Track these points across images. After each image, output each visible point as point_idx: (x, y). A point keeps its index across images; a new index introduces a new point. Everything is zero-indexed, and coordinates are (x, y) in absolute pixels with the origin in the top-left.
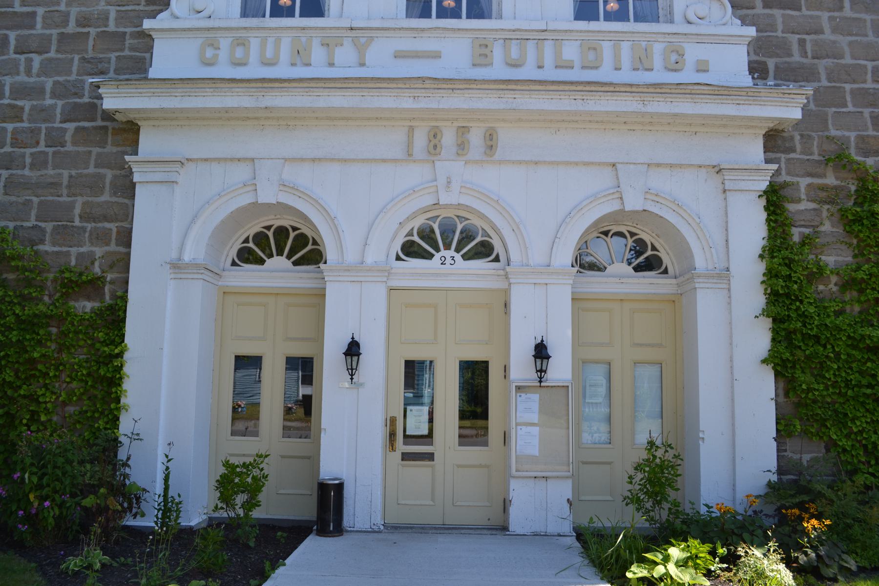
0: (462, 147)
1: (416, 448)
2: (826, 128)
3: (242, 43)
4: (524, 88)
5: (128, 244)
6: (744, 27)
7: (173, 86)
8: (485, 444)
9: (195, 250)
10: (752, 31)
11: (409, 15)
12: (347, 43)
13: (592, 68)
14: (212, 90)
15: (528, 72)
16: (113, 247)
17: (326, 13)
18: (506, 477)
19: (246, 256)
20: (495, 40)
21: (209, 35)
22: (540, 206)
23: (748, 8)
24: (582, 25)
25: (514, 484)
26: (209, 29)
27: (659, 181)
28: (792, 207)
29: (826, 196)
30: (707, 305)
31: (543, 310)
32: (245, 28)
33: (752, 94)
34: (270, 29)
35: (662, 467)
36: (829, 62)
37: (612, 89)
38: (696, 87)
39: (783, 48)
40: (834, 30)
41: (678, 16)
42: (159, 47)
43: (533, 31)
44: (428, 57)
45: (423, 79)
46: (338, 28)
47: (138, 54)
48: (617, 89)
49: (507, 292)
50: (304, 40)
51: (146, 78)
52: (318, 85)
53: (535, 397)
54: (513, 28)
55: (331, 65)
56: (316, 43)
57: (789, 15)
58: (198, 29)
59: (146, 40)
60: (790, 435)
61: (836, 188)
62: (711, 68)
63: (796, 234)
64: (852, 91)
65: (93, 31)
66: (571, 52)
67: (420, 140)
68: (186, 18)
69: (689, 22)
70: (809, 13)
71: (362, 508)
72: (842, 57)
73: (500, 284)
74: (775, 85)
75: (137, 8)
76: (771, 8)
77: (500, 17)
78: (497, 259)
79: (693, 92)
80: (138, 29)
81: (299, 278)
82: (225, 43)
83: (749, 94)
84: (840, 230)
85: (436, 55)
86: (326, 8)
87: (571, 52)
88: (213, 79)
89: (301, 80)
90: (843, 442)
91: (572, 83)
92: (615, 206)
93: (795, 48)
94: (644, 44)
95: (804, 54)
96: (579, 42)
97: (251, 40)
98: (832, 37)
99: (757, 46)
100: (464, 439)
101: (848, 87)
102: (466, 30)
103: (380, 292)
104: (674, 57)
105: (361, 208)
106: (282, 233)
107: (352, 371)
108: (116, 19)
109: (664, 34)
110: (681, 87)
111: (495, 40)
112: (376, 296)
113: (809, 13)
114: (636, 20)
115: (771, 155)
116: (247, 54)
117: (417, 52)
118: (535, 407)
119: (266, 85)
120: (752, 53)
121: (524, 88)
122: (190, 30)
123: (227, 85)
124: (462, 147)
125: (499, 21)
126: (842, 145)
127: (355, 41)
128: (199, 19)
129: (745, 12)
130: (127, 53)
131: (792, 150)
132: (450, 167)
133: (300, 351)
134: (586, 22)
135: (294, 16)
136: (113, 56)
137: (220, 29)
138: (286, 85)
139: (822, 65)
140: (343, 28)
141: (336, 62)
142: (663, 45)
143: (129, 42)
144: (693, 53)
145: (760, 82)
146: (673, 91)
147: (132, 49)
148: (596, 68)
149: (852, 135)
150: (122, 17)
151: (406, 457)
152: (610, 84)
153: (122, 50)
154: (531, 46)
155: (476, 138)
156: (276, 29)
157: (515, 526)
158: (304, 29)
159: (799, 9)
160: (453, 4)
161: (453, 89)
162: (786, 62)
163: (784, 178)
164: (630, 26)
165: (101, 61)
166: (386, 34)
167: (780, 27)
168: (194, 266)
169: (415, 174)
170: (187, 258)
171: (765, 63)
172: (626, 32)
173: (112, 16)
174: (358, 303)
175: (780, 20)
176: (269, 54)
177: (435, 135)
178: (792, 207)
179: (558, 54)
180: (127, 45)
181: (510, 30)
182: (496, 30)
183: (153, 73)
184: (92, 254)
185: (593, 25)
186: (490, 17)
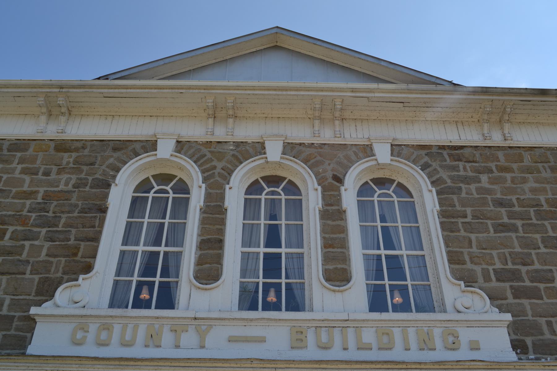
3: (107, 328)
4: (333, 367)
6: (502, 314)
7: (46, 362)
10: (508, 317)
11: (241, 308)
12: (191, 330)
13: (387, 349)
14: (77, 366)
15: (336, 353)
17: (176, 306)
20: (309, 327)
23: (502, 299)
24: (376, 316)
26: (82, 316)
32: (111, 316)
33: (518, 367)
34: (131, 317)
37: (404, 366)
38: (472, 363)
39: (535, 329)
41: (449, 307)
42: (40, 330)
43: (337, 320)
44: (256, 341)
45: (251, 360)
46: (185, 318)
47: (21, 333)
48: (409, 367)
50: (157, 326)
51: (24, 354)
52: (165, 364)
54: (322, 318)
55: (177, 347)
56: (166, 329)
57: (534, 303)
58: (73, 316)
59: (31, 323)
62: (481, 346)
66: (369, 336)
68: (65, 307)
69: (459, 312)
70: (549, 301)
74: (537, 359)
75: (27, 297)
76: (519, 298)
77: (312, 310)
79: (471, 367)
80: (26, 314)
82: (93, 328)
83: (517, 367)
85: (262, 340)
86: (176, 302)
87: (369, 336)
88: (80, 357)
89: (152, 360)
91: (372, 362)
93: (545, 328)
94: (426, 329)
96: (374, 329)
97: (115, 325)
99: (515, 328)
102: (286, 320)
104: (451, 339)
108: (9, 305)
109: (441, 321)
110: (460, 363)
111: (309, 327)
113: (549, 301)
114: (418, 311)
117: (247, 337)
119: (122, 363)
120: (512, 333)
121: (333, 367)
122: (66, 316)
123: (91, 362)
125: (311, 313)
128: (76, 308)
129: (499, 302)
130: (13, 332)
134: (378, 314)
135: (150, 308)
137: (91, 316)
138: (139, 363)
140: (188, 318)
141: (181, 345)
142: (442, 329)
143: (16, 323)
144: (466, 335)
145: (523, 357)
146: (454, 367)
147: (17, 329)
148: (390, 349)
150: (14, 305)
152: (403, 363)
153: (9, 330)
154: (337, 333)
156: (136, 317)
158: (158, 318)
159: (542, 299)
160: (275, 300)
161: (275, 368)
162: (540, 340)
164: (413, 316)
166: (223, 323)
167: (530, 313)
171: (523, 341)
172: (410, 321)
175: (528, 308)
179: (359, 338)
180: (14, 326)
181: (319, 320)
182: (309, 320)
183: (30, 350)
185: (384, 316)
186: (303, 310)
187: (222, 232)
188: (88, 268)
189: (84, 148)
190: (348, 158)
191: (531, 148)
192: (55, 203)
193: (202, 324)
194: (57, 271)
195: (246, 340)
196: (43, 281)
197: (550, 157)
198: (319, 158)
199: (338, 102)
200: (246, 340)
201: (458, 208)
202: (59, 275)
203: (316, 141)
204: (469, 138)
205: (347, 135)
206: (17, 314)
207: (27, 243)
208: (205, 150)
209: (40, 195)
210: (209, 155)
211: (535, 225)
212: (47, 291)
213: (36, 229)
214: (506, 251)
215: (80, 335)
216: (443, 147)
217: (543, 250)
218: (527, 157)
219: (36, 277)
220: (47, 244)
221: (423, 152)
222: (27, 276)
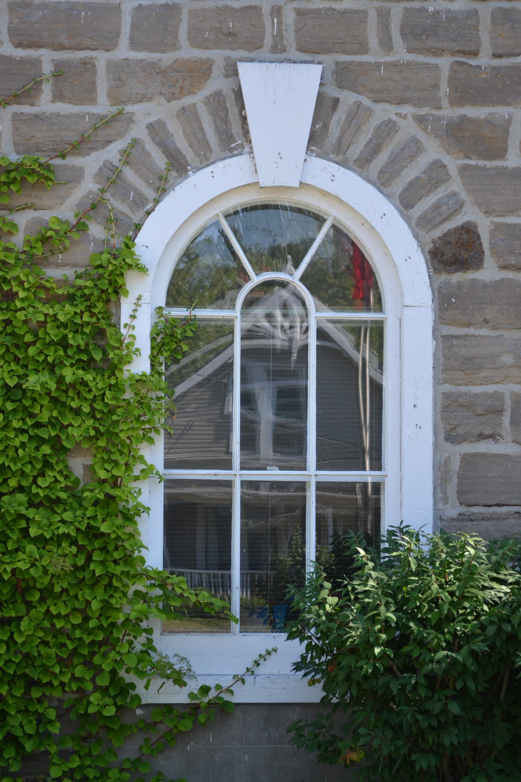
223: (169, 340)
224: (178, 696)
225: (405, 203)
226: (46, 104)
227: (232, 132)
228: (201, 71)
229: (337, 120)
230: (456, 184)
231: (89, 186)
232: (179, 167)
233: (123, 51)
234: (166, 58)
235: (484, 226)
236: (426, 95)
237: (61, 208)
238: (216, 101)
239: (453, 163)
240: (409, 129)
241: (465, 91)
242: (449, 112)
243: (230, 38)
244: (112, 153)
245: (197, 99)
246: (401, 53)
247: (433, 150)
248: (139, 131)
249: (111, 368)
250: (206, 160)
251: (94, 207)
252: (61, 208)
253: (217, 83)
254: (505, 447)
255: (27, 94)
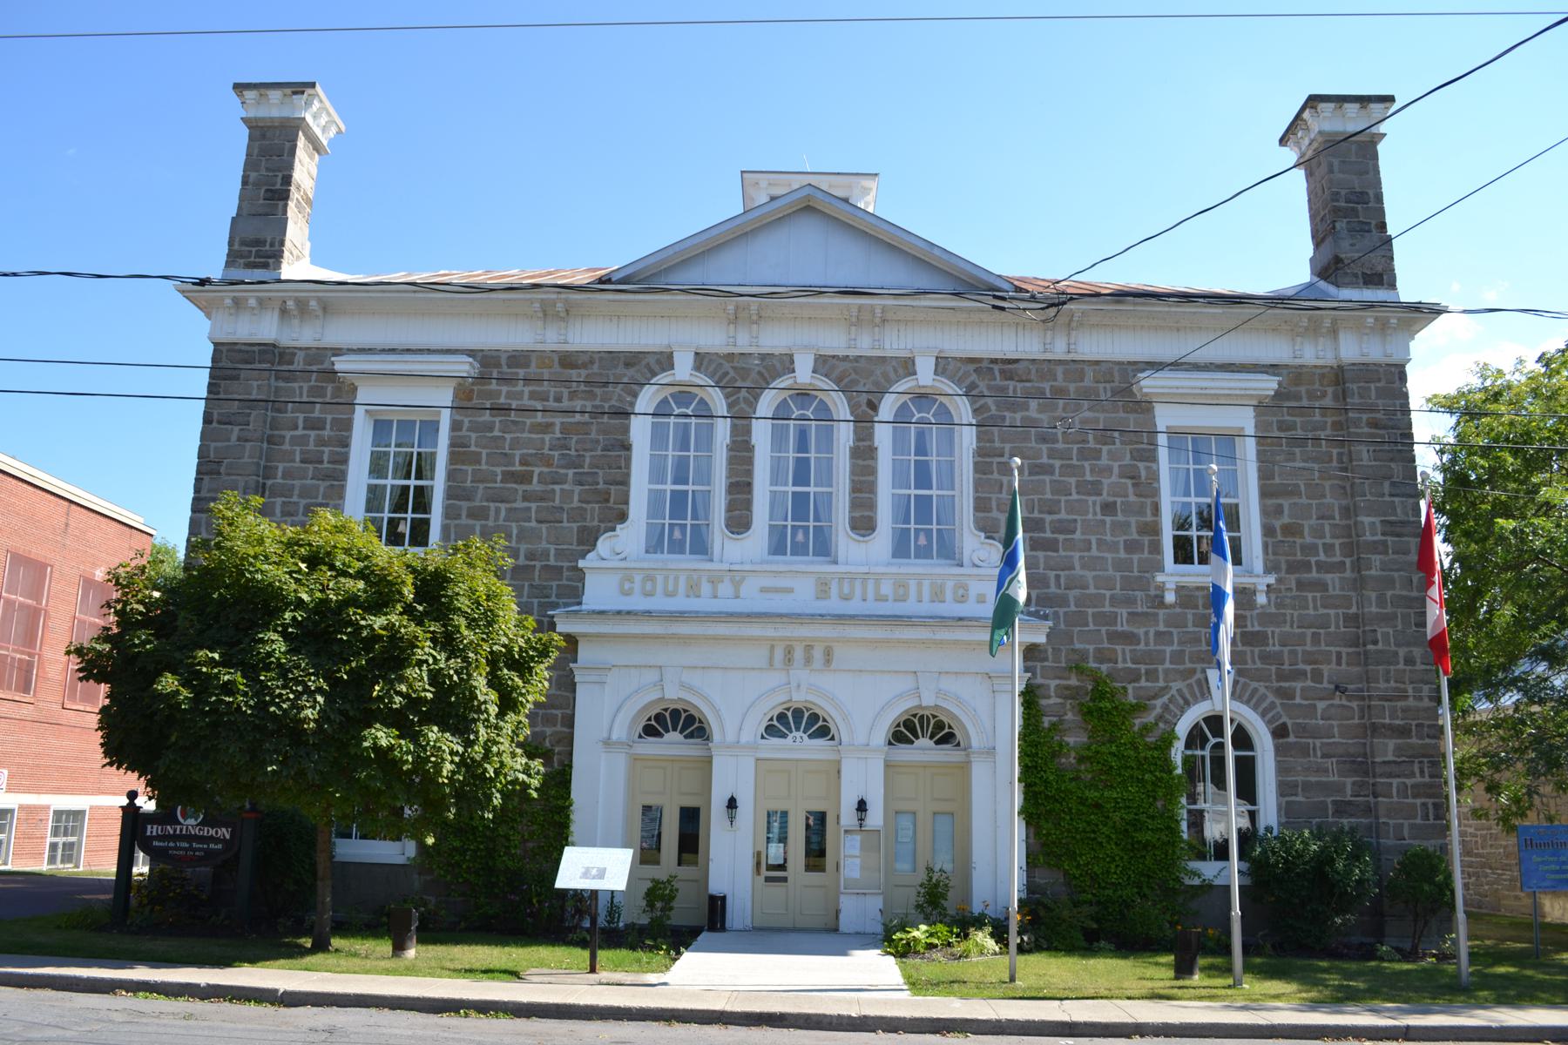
0: (808, 660)
1: (776, 872)
2: (1072, 642)
3: (652, 579)
5: (572, 726)
8: (823, 870)
9: (619, 733)
12: (727, 580)
16: (559, 728)
18: (838, 893)
19: (649, 731)
21: (627, 575)
22: (864, 702)
25: (843, 898)
27: (947, 684)
28: (1043, 702)
29: (1068, 693)
30: (980, 773)
31: (863, 775)
35: (937, 885)
36: (1077, 592)
40: (1083, 567)
41: (966, 561)
42: (590, 580)
49: (839, 762)
53: (858, 838)
59: (580, 575)
60: (1036, 866)
61: (1077, 687)
62: (818, 807)
63: (1046, 722)
64: (1094, 615)
65: (538, 564)
66: (886, 588)
67: (779, 654)
71: (739, 912)
72: (1087, 587)
73: (833, 757)
78: (833, 739)
81: (692, 749)
82: (638, 578)
84: (1079, 718)
90: (1077, 873)
92: (916, 703)
93: (1052, 581)
95: (1059, 586)
98: (1081, 573)
100: (808, 868)
101: (1090, 611)
103: (752, 760)
104: (961, 592)
105: (737, 701)
106: (676, 713)
107: (732, 819)
112: (747, 765)
115: (1030, 664)
116: (654, 587)
118: (858, 844)
124: (808, 660)
126: (1084, 656)
127: (732, 580)
131: (1046, 659)
132: (800, 674)
133: (690, 802)
136: (554, 584)
139: (1072, 594)
143: (566, 574)
149: (1091, 648)
151: (768, 879)
155: (818, 654)
157: (843, 927)
163: (1039, 680)
165: (545, 587)
168: (619, 743)
169: (775, 678)
170: (614, 737)
173: (552, 553)
174: (733, 774)
176: (671, 588)
177: (789, 651)
178: (1043, 702)
184: (543, 733)
187: (750, 473)
188: (623, 517)
189: (592, 362)
190: (885, 375)
191: (1097, 363)
192: (575, 438)
193: (737, 577)
194: (593, 519)
195: (777, 590)
196: (582, 530)
197: (1116, 374)
198: (853, 376)
199: (878, 311)
200: (777, 590)
201: (997, 444)
202: (596, 523)
203: (852, 353)
204: (1028, 349)
205: (887, 346)
206: (566, 564)
207: (557, 487)
208: (727, 366)
209: (557, 429)
210: (732, 373)
211: (1074, 466)
212: (588, 540)
213: (562, 471)
214: (1036, 497)
215: (626, 586)
216: (994, 361)
217: (1075, 496)
218: (1090, 374)
219: (575, 526)
220: (577, 489)
221: (971, 367)
222: (565, 524)
223: (1187, 760)
224: (1196, 882)
225: (1263, 715)
226: (1143, 683)
227: (1204, 691)
228: (1193, 672)
229: (1239, 687)
230: (1279, 709)
231: (1158, 710)
232: (1188, 704)
233: (1167, 665)
234: (1181, 667)
235: (1289, 723)
236: (1268, 679)
237: (1150, 718)
238: (1199, 682)
239: (1278, 702)
240: (1262, 690)
241: (1281, 676)
242: (1275, 684)
243: (1202, 660)
244: (1165, 699)
245: (1192, 681)
246: (1259, 665)
247: (1271, 698)
248: (1173, 692)
249: (1170, 772)
250: (1196, 702)
251: (1160, 717)
252: (1150, 718)
253: (1199, 675)
254: (1300, 799)
255: (1137, 680)
